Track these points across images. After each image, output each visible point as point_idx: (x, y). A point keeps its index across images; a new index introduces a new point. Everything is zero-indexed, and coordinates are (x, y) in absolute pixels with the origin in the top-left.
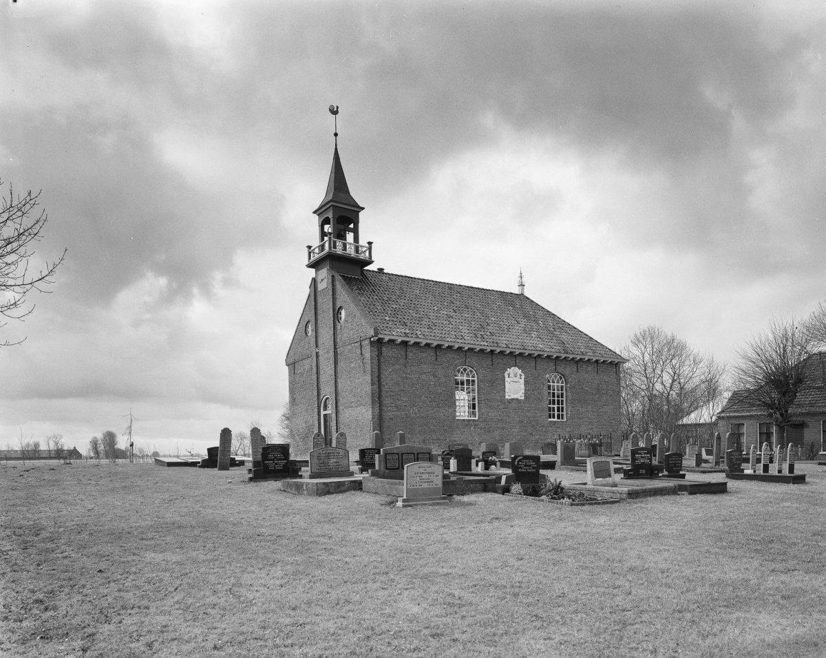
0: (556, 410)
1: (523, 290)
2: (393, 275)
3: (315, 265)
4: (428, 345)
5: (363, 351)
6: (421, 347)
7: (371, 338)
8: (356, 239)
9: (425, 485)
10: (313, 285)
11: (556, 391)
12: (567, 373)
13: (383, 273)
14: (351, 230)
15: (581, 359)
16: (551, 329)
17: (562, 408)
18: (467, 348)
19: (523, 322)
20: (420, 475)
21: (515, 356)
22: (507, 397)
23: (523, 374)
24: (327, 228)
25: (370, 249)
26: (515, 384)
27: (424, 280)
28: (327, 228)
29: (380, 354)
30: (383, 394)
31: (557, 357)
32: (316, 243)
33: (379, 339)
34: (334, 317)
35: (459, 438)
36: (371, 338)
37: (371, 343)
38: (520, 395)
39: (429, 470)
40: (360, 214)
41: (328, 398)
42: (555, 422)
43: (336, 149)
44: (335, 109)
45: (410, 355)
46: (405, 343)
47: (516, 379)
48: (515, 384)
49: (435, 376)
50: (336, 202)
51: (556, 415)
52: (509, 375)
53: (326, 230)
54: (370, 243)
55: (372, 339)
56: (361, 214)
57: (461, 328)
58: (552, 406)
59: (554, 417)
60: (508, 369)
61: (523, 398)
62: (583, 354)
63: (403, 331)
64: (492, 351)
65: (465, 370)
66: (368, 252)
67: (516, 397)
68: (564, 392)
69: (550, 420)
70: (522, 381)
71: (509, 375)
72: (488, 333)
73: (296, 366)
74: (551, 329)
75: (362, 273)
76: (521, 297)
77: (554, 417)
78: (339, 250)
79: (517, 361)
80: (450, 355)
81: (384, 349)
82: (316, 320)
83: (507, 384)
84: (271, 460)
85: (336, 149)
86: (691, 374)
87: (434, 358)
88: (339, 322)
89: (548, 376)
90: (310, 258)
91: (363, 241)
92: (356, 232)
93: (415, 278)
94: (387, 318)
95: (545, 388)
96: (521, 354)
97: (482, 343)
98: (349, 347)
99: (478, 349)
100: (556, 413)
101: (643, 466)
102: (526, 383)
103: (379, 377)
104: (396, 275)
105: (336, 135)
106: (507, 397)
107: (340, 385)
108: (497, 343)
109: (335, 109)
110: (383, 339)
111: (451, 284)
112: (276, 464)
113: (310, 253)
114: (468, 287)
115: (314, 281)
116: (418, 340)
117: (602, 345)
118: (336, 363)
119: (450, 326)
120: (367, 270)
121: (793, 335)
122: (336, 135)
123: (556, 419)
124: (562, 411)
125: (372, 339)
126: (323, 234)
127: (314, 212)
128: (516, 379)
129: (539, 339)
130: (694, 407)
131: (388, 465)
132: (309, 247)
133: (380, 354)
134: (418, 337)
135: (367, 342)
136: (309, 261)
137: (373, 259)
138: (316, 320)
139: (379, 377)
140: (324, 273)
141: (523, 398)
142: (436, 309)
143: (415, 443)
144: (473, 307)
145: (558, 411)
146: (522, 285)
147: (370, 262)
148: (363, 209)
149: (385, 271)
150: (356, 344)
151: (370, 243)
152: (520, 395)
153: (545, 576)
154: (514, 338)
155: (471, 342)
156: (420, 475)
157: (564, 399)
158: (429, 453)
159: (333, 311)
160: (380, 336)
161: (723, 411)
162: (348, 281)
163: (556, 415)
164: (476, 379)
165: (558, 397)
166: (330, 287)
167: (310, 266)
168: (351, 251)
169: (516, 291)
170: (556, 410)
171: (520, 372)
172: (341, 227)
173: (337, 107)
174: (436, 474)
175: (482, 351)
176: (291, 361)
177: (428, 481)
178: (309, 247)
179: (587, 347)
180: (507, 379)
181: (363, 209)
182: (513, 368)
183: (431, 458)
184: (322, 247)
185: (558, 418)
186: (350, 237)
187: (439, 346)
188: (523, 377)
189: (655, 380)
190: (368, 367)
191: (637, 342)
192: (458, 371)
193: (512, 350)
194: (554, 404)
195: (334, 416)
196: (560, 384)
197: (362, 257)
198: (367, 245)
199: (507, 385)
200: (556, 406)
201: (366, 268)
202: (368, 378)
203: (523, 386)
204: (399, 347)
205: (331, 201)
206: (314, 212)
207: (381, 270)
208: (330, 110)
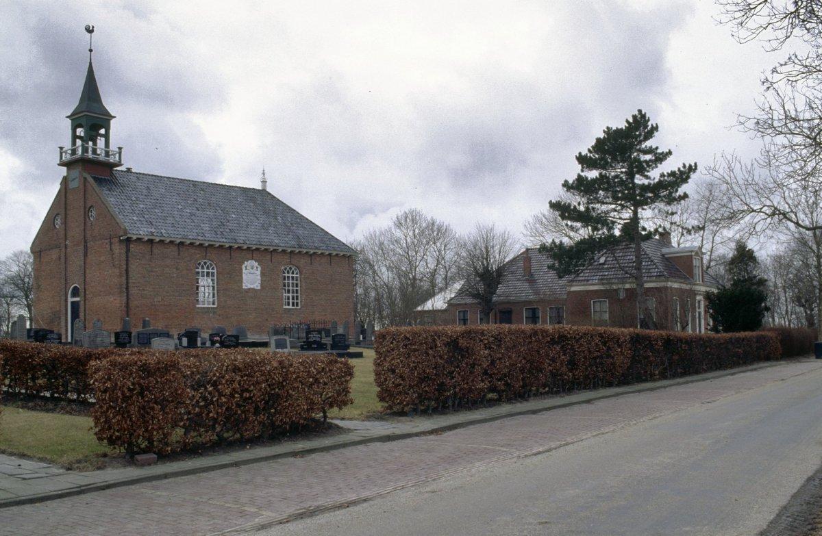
0: (291, 298)
2: (140, 174)
3: (68, 165)
4: (171, 242)
5: (113, 247)
8: (107, 144)
13: (131, 172)
14: (102, 135)
15: (314, 253)
16: (289, 225)
18: (207, 244)
19: (262, 218)
21: (253, 250)
24: (80, 132)
25: (120, 153)
26: (251, 276)
27: (170, 178)
28: (80, 132)
29: (128, 251)
30: (131, 285)
31: (292, 252)
32: (68, 145)
34: (85, 212)
35: (196, 324)
38: (257, 285)
39: (167, 343)
40: (111, 121)
42: (290, 309)
43: (91, 64)
44: (91, 28)
45: (155, 250)
46: (151, 241)
47: (252, 271)
48: (251, 276)
49: (177, 269)
50: (88, 112)
51: (291, 303)
52: (246, 267)
53: (78, 134)
56: (113, 122)
57: (202, 225)
59: (289, 305)
61: (259, 288)
62: (317, 248)
63: (150, 230)
64: (230, 247)
65: (205, 263)
66: (118, 155)
67: (252, 287)
70: (259, 273)
71: (246, 267)
72: (228, 230)
73: (42, 254)
74: (289, 225)
75: (112, 175)
76: (263, 192)
77: (289, 305)
78: (90, 155)
80: (192, 250)
81: (132, 246)
83: (244, 275)
85: (91, 64)
87: (176, 253)
89: (283, 268)
91: (113, 147)
92: (107, 136)
93: (161, 177)
94: (135, 218)
95: (281, 279)
96: (257, 249)
97: (221, 240)
98: (100, 242)
99: (217, 245)
100: (291, 301)
101: (315, 342)
102: (262, 274)
104: (143, 174)
105: (91, 51)
107: (88, 276)
108: (235, 239)
109: (91, 28)
110: (131, 238)
111: (196, 182)
113: (61, 154)
114: (212, 184)
115: (65, 179)
116: (162, 238)
117: (336, 239)
118: (86, 255)
119: (193, 224)
120: (116, 170)
121: (487, 237)
122: (91, 51)
123: (291, 307)
124: (297, 299)
126: (75, 137)
127: (67, 117)
128: (252, 271)
129: (276, 235)
130: (430, 294)
132: (61, 148)
133: (128, 251)
134: (162, 236)
135: (117, 240)
136: (60, 161)
137: (122, 163)
140: (76, 172)
141: (259, 288)
142: (180, 207)
143: (160, 326)
144: (215, 205)
145: (293, 299)
146: (264, 182)
147: (120, 164)
148: (115, 117)
149: (133, 171)
150: (106, 241)
151: (120, 148)
152: (257, 285)
154: (249, 235)
155: (212, 239)
158: (168, 334)
160: (129, 235)
162: (99, 181)
163: (291, 303)
164: (215, 271)
166: (82, 187)
167: (62, 164)
169: (259, 186)
170: (291, 298)
171: (256, 264)
172: (94, 133)
173: (93, 27)
175: (221, 247)
176: (37, 250)
178: (61, 148)
179: (322, 241)
180: (244, 271)
181: (115, 117)
182: (249, 262)
183: (168, 335)
184: (74, 152)
185: (293, 305)
186: (101, 142)
187: (182, 243)
188: (259, 269)
189: (417, 263)
191: (399, 224)
192: (199, 264)
193: (249, 246)
194: (293, 290)
195: (82, 302)
197: (112, 160)
198: (117, 150)
199: (244, 276)
200: (291, 295)
201: (115, 169)
203: (259, 277)
207: (129, 170)
208: (86, 29)
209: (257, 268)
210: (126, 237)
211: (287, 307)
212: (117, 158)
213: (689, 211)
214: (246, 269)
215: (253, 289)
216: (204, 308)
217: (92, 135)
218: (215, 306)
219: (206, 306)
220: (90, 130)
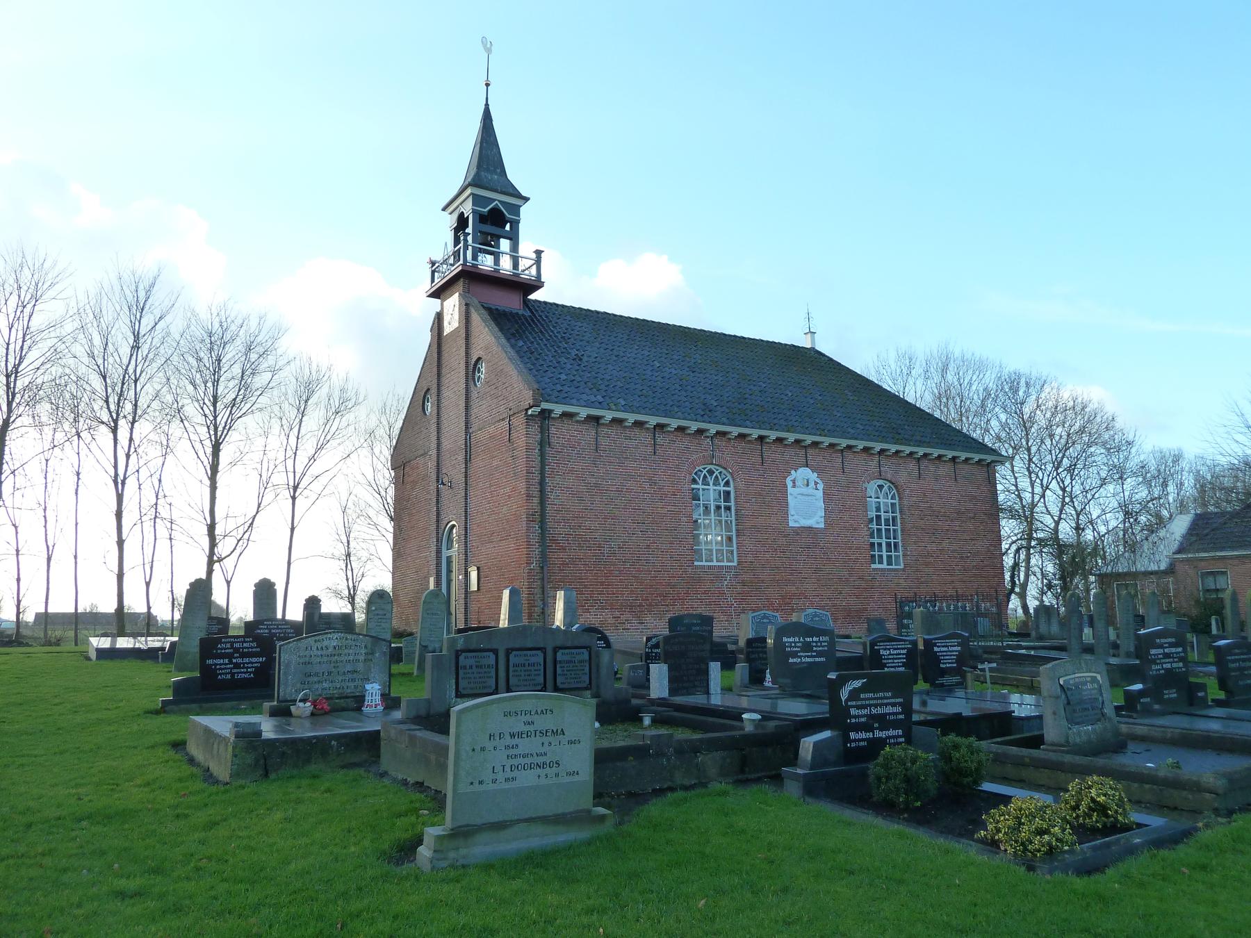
1: (813, 341)
5: (514, 435)
6: (626, 427)
7: (527, 410)
8: (515, 247)
9: (528, 778)
10: (436, 325)
11: (882, 514)
12: (902, 478)
17: (896, 544)
20: (508, 741)
22: (791, 524)
23: (819, 481)
25: (538, 262)
29: (544, 443)
33: (543, 411)
34: (467, 374)
36: (527, 410)
37: (529, 418)
38: (816, 520)
39: (543, 723)
40: (521, 208)
41: (453, 526)
43: (487, 105)
49: (653, 483)
54: (539, 253)
55: (530, 412)
56: (525, 210)
58: (876, 540)
59: (881, 562)
60: (793, 472)
61: (822, 526)
65: (711, 472)
68: (898, 515)
69: (873, 566)
70: (820, 494)
77: (881, 562)
79: (810, 457)
82: (439, 385)
84: (222, 656)
85: (487, 105)
86: (316, 679)
88: (475, 385)
90: (433, 281)
92: (514, 238)
100: (884, 554)
102: (826, 495)
103: (542, 483)
105: (487, 85)
106: (791, 524)
110: (550, 411)
112: (237, 666)
113: (433, 272)
115: (439, 317)
123: (885, 566)
125: (530, 412)
131: (462, 684)
132: (433, 263)
138: (439, 385)
139: (542, 483)
141: (822, 526)
147: (536, 285)
148: (527, 199)
149: (489, 88)
151: (539, 253)
152: (816, 520)
153: (754, 385)
156: (508, 741)
157: (899, 528)
159: (467, 367)
160: (545, 405)
161: (1179, 551)
164: (731, 489)
165: (887, 524)
168: (506, 264)
171: (813, 476)
174: (570, 735)
177: (540, 760)
178: (433, 263)
180: (790, 490)
181: (527, 199)
182: (801, 470)
185: (889, 563)
188: (821, 486)
190: (521, 462)
194: (880, 537)
196: (890, 501)
198: (534, 256)
199: (791, 501)
200: (884, 541)
202: (522, 486)
204: (585, 427)
205: (469, 185)
206: (444, 209)
209: (816, 483)
210: (538, 409)
211: (880, 566)
212: (533, 271)
213: (379, 624)
214: (794, 486)
215: (810, 528)
216: (710, 567)
217: (488, 242)
218: (735, 564)
219: (715, 563)
220: (480, 222)
